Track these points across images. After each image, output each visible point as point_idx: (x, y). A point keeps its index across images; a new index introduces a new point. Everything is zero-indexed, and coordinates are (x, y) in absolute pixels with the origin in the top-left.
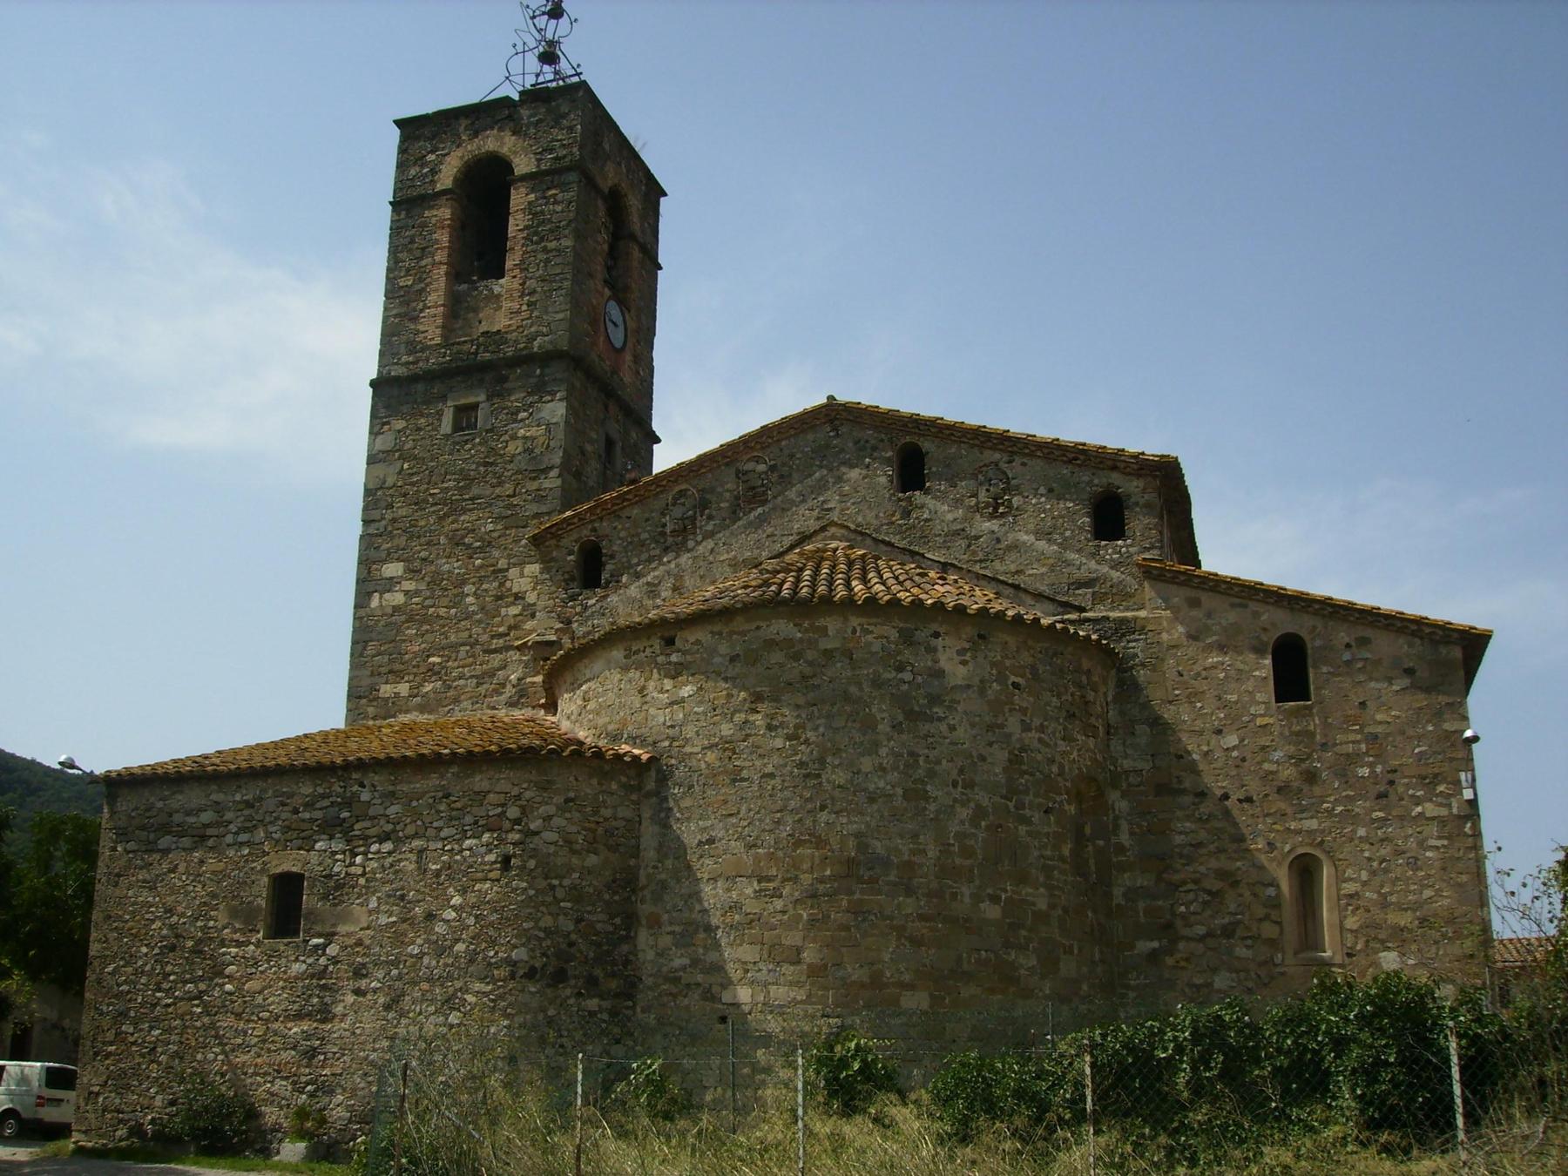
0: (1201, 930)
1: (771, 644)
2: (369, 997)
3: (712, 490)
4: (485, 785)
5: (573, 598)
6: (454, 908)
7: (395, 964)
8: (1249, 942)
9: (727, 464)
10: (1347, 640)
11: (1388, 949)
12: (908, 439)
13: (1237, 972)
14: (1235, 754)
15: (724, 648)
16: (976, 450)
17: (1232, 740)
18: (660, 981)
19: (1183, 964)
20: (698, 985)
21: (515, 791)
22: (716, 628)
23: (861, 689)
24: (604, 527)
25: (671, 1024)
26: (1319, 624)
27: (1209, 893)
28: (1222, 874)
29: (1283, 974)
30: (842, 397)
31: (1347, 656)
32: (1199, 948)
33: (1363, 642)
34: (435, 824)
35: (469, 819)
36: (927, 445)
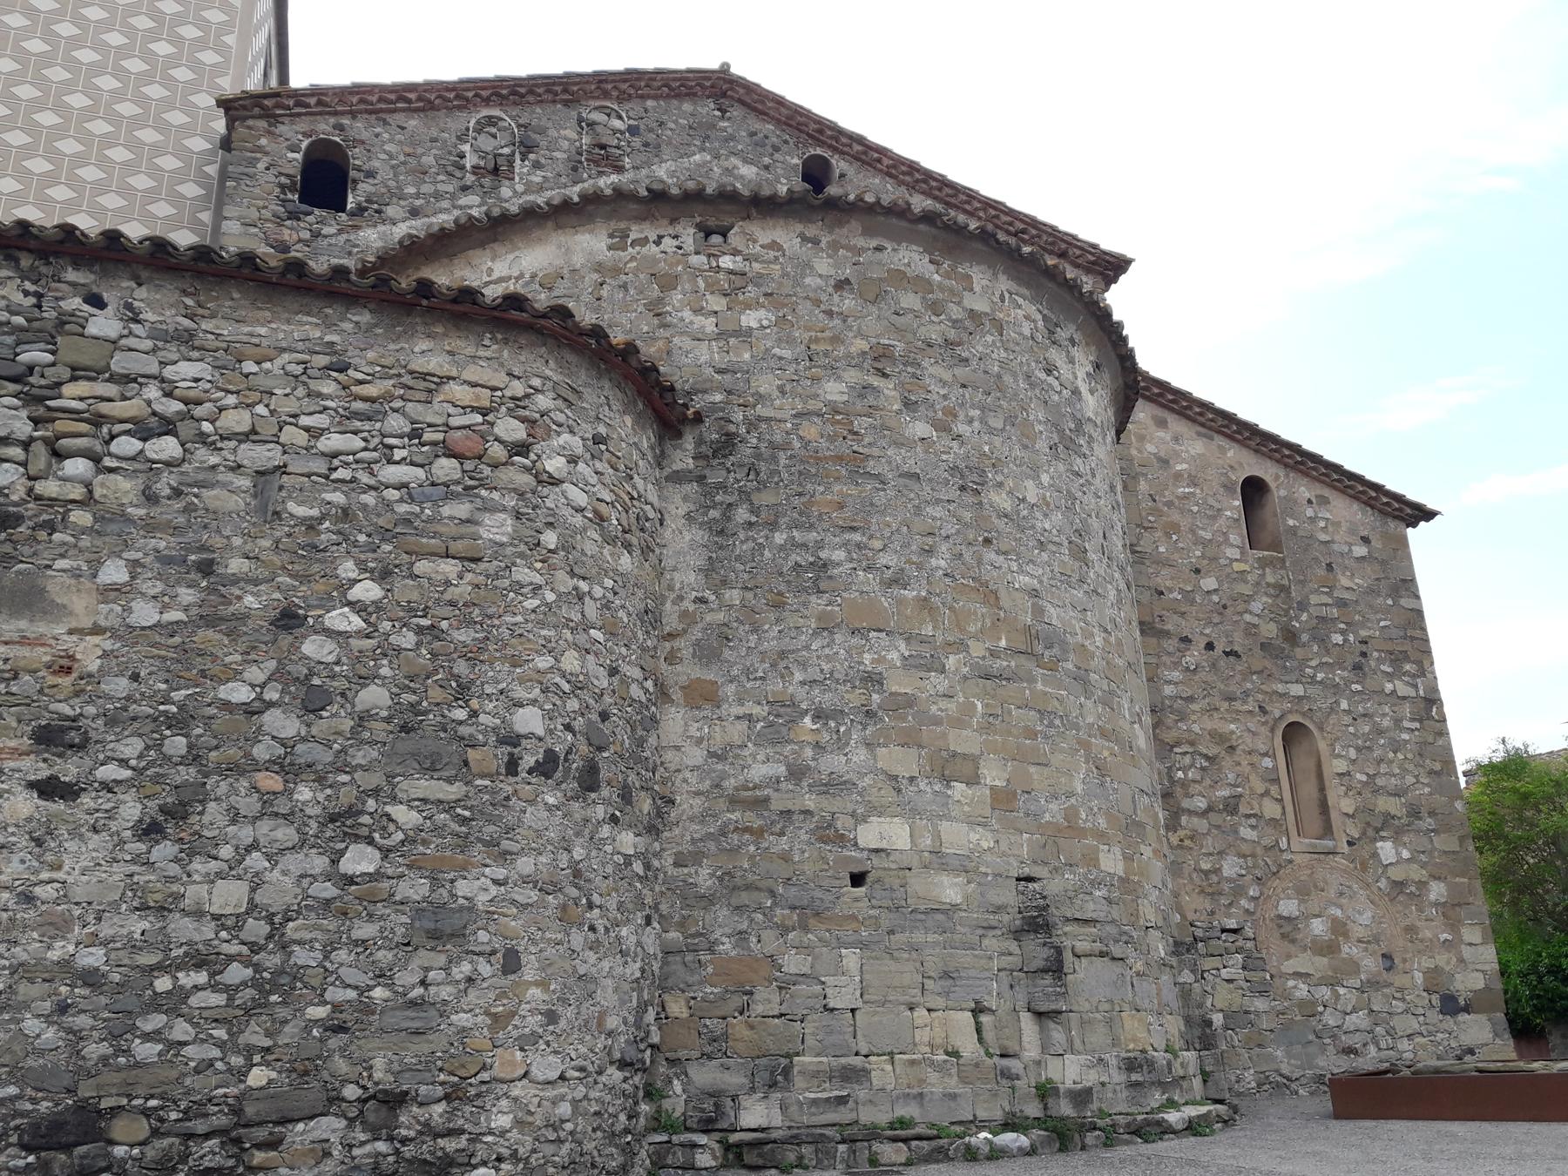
0: (1201, 803)
1: (900, 278)
2: (86, 800)
3: (542, 131)
4: (435, 363)
5: (294, 216)
6: (358, 607)
7: (179, 722)
8: (1253, 821)
9: (566, 103)
10: (1307, 495)
11: (1383, 839)
12: (819, 151)
13: (1245, 856)
14: (1215, 598)
15: (823, 265)
16: (903, 188)
17: (1209, 583)
18: (722, 804)
19: (1187, 843)
20: (807, 812)
21: (518, 388)
22: (812, 230)
23: (1016, 381)
24: (359, 127)
25: (749, 887)
26: (1282, 473)
27: (1207, 757)
28: (1219, 737)
29: (1291, 862)
30: (736, 70)
31: (1310, 512)
32: (1201, 825)
33: (1324, 501)
34: (305, 421)
35: (396, 423)
36: (839, 165)
